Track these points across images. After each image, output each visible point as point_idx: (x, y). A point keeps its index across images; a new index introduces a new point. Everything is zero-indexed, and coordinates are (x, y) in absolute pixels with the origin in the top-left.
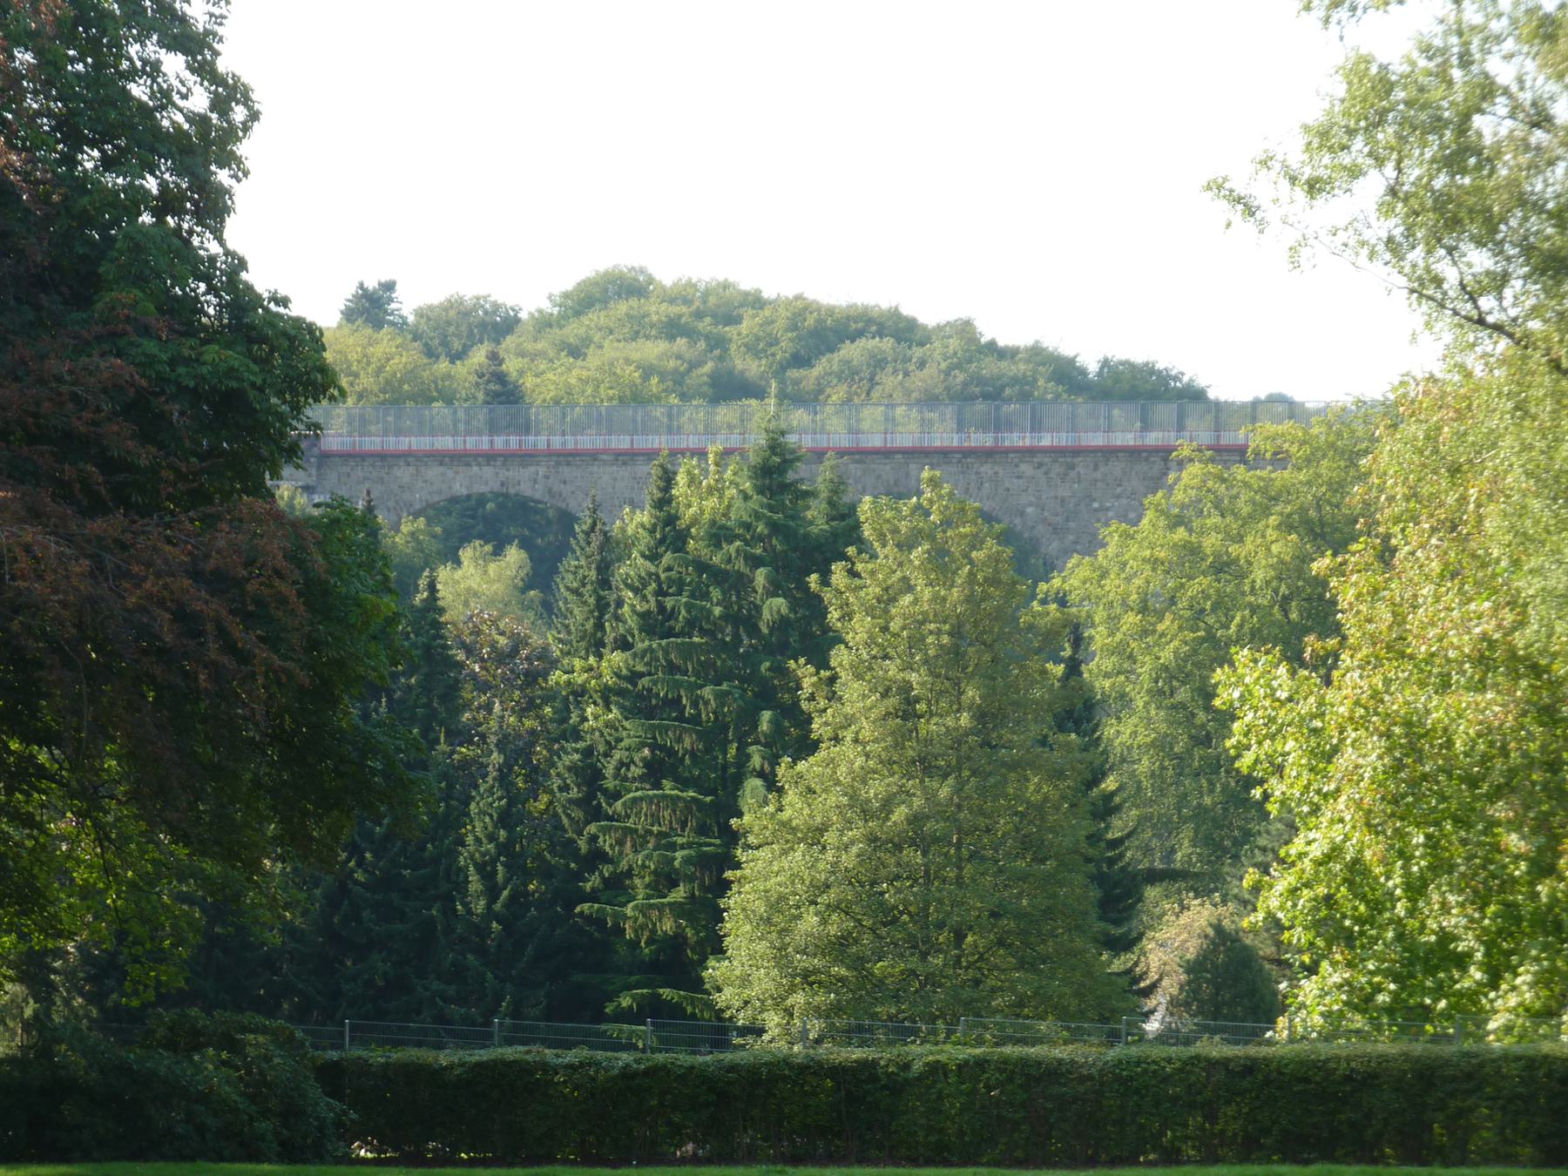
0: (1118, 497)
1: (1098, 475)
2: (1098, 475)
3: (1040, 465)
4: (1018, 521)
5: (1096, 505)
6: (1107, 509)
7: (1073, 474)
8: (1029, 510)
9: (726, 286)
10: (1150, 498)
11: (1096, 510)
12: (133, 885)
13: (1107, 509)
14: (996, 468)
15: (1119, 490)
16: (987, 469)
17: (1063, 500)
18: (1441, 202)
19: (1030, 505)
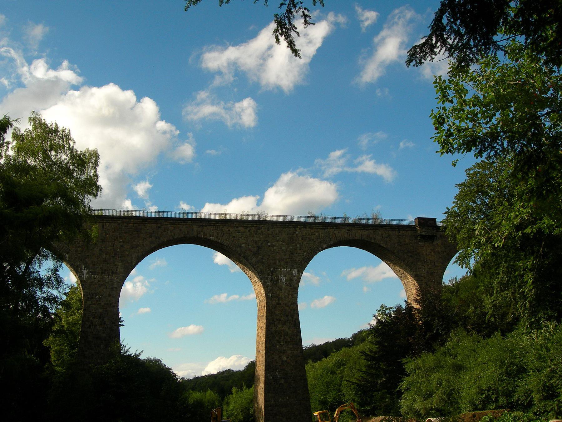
0: (278, 241)
1: (270, 232)
2: (270, 232)
3: (247, 228)
4: (239, 249)
5: (269, 244)
6: (274, 246)
7: (260, 231)
8: (243, 245)
9: (98, 88)
10: (53, 158)
11: (269, 246)
12: (56, 152)
13: (274, 246)
14: (229, 228)
15: (278, 238)
16: (225, 229)
17: (256, 242)
18: (479, 152)
19: (243, 243)
